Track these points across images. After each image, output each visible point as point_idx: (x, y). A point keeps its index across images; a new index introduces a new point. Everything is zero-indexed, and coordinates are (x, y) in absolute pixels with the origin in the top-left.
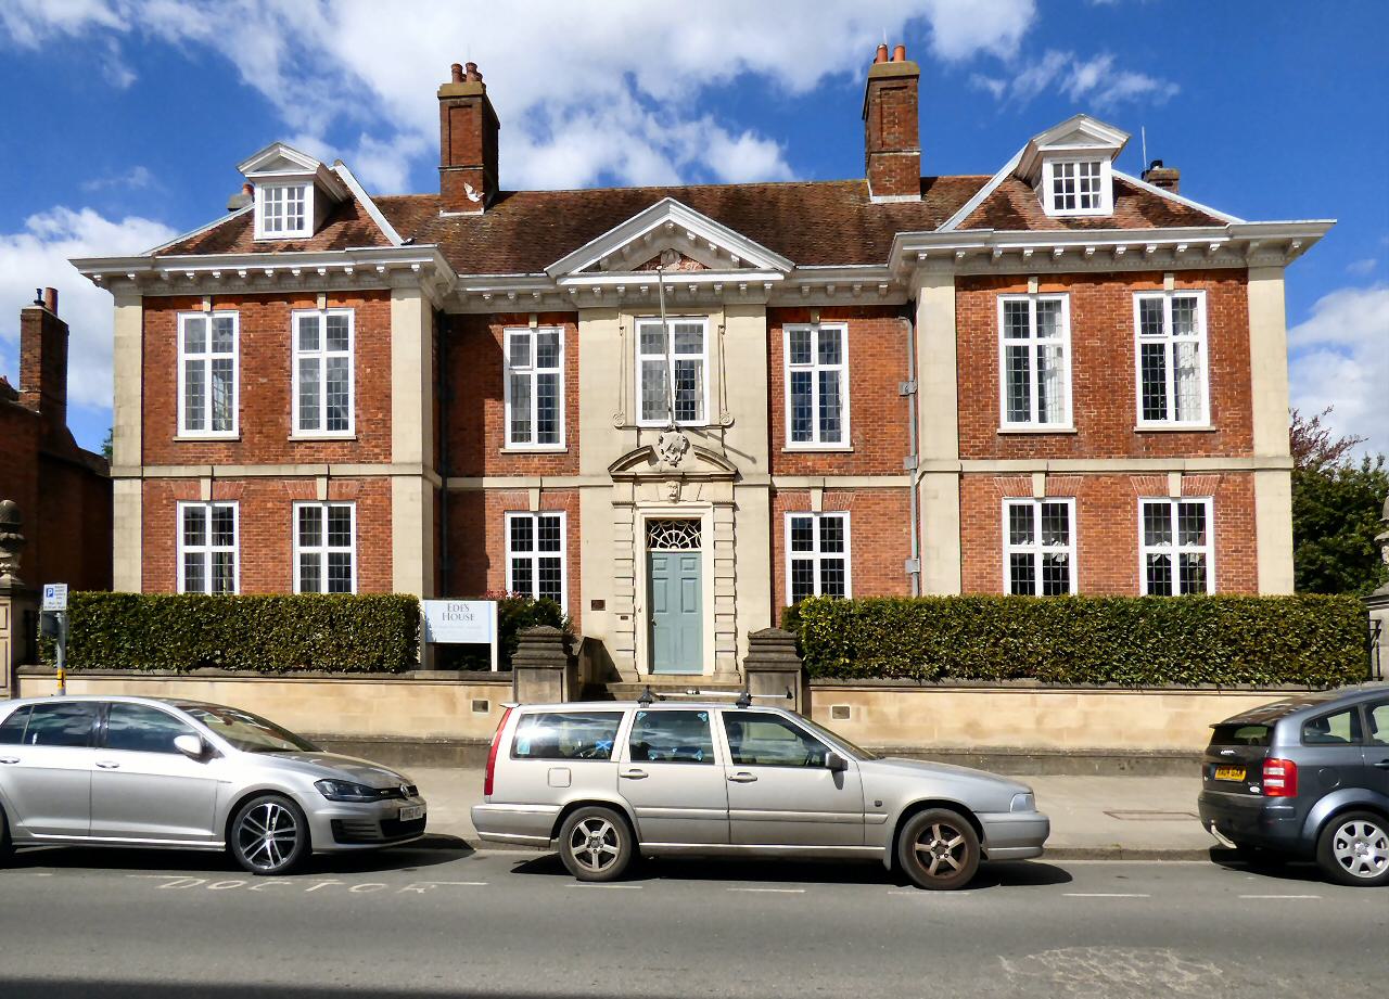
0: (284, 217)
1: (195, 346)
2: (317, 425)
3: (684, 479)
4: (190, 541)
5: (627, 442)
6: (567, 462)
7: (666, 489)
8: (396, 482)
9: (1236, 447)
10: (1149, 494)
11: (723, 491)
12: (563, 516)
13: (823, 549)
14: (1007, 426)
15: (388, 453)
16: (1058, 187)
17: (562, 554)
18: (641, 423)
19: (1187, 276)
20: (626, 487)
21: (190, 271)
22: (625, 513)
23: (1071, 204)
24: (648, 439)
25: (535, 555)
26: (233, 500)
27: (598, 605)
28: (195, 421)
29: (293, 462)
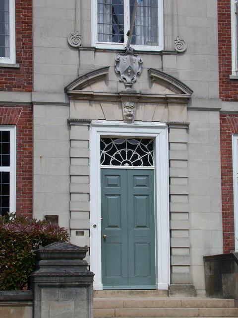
12: (13, 132)
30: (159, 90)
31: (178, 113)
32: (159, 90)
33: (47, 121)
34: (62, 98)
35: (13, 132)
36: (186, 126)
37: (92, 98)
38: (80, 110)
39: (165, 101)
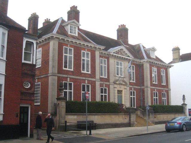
8: (96, 82)
17: (107, 94)
19: (71, 46)
23: (72, 33)
29: (82, 76)
30: (124, 83)
31: (125, 87)
32: (124, 83)
33: (111, 87)
34: (113, 84)
35: (107, 88)
36: (126, 89)
37: (116, 84)
38: (115, 86)
39: (124, 85)
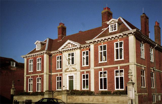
0: (113, 29)
1: (117, 46)
2: (118, 58)
3: (71, 71)
4: (57, 80)
5: (66, 67)
6: (61, 71)
7: (70, 73)
9: (127, 62)
10: (116, 69)
11: (75, 72)
13: (86, 78)
14: (100, 62)
15: (129, 61)
16: (116, 27)
18: (68, 65)
20: (66, 73)
21: (38, 54)
22: (66, 76)
24: (68, 67)
25: (85, 79)
26: (106, 70)
27: (64, 86)
28: (38, 70)
